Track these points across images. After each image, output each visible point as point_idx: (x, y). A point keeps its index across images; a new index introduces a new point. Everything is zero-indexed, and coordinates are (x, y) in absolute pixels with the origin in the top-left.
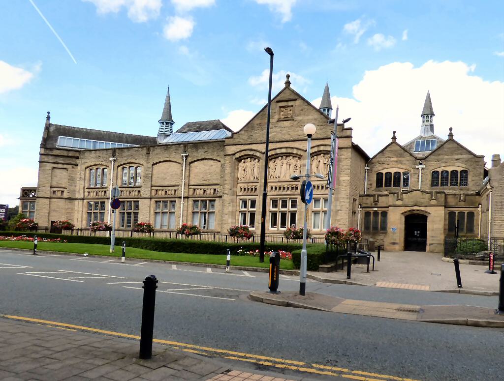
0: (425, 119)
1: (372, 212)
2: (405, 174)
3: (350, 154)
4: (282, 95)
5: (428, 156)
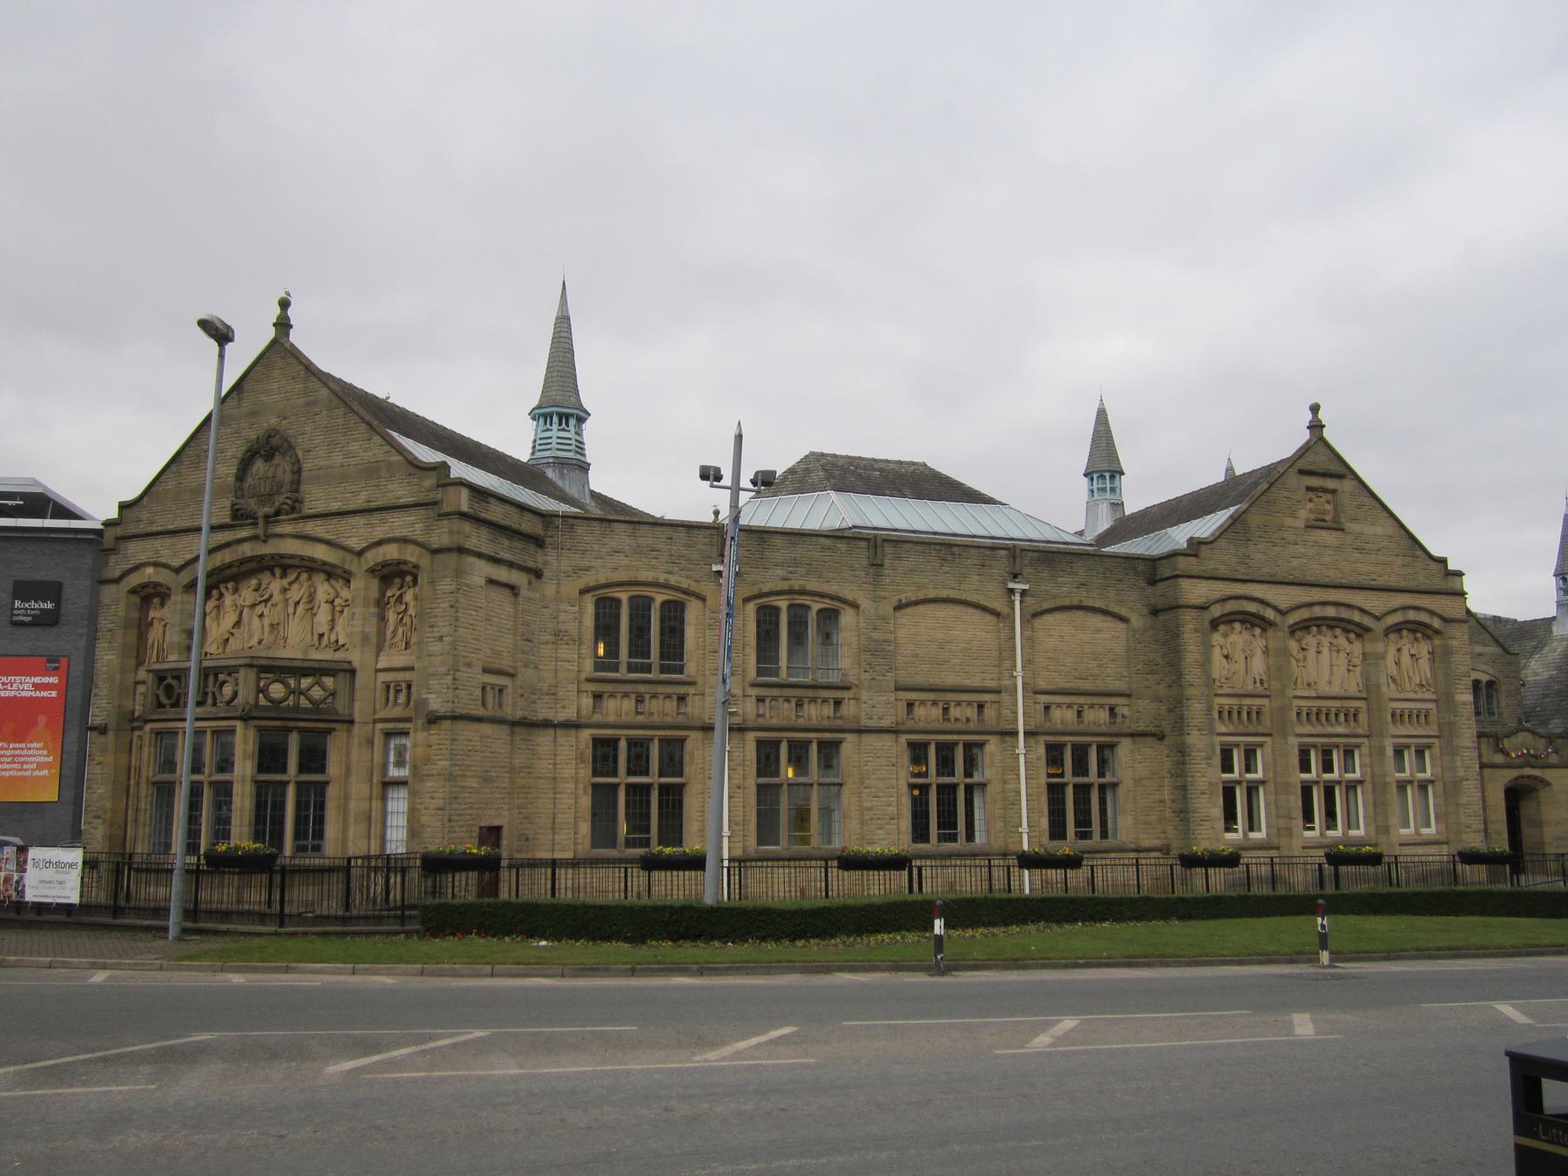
4: (1310, 457)
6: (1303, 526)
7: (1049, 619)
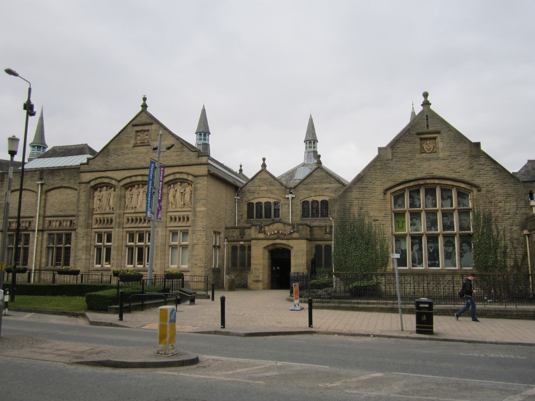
0: (308, 145)
1: (238, 246)
2: (276, 204)
3: (206, 182)
4: (138, 119)
5: (298, 185)
6: (132, 146)
7: (53, 192)
